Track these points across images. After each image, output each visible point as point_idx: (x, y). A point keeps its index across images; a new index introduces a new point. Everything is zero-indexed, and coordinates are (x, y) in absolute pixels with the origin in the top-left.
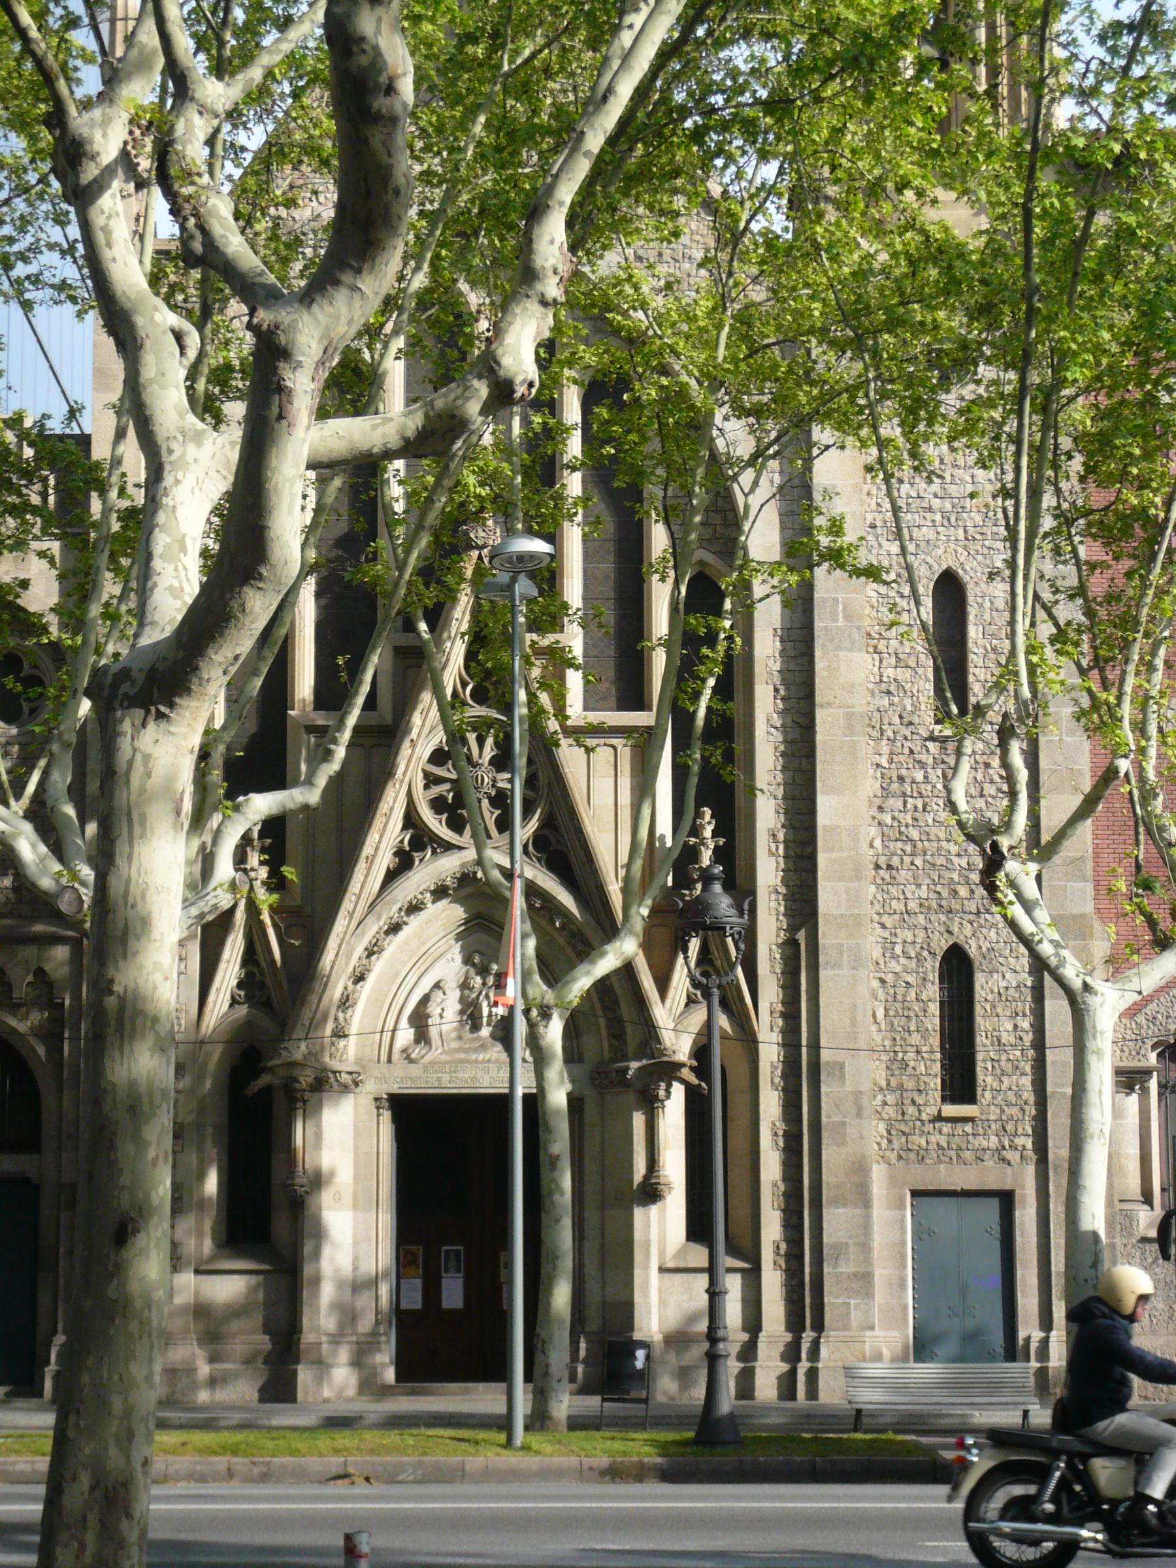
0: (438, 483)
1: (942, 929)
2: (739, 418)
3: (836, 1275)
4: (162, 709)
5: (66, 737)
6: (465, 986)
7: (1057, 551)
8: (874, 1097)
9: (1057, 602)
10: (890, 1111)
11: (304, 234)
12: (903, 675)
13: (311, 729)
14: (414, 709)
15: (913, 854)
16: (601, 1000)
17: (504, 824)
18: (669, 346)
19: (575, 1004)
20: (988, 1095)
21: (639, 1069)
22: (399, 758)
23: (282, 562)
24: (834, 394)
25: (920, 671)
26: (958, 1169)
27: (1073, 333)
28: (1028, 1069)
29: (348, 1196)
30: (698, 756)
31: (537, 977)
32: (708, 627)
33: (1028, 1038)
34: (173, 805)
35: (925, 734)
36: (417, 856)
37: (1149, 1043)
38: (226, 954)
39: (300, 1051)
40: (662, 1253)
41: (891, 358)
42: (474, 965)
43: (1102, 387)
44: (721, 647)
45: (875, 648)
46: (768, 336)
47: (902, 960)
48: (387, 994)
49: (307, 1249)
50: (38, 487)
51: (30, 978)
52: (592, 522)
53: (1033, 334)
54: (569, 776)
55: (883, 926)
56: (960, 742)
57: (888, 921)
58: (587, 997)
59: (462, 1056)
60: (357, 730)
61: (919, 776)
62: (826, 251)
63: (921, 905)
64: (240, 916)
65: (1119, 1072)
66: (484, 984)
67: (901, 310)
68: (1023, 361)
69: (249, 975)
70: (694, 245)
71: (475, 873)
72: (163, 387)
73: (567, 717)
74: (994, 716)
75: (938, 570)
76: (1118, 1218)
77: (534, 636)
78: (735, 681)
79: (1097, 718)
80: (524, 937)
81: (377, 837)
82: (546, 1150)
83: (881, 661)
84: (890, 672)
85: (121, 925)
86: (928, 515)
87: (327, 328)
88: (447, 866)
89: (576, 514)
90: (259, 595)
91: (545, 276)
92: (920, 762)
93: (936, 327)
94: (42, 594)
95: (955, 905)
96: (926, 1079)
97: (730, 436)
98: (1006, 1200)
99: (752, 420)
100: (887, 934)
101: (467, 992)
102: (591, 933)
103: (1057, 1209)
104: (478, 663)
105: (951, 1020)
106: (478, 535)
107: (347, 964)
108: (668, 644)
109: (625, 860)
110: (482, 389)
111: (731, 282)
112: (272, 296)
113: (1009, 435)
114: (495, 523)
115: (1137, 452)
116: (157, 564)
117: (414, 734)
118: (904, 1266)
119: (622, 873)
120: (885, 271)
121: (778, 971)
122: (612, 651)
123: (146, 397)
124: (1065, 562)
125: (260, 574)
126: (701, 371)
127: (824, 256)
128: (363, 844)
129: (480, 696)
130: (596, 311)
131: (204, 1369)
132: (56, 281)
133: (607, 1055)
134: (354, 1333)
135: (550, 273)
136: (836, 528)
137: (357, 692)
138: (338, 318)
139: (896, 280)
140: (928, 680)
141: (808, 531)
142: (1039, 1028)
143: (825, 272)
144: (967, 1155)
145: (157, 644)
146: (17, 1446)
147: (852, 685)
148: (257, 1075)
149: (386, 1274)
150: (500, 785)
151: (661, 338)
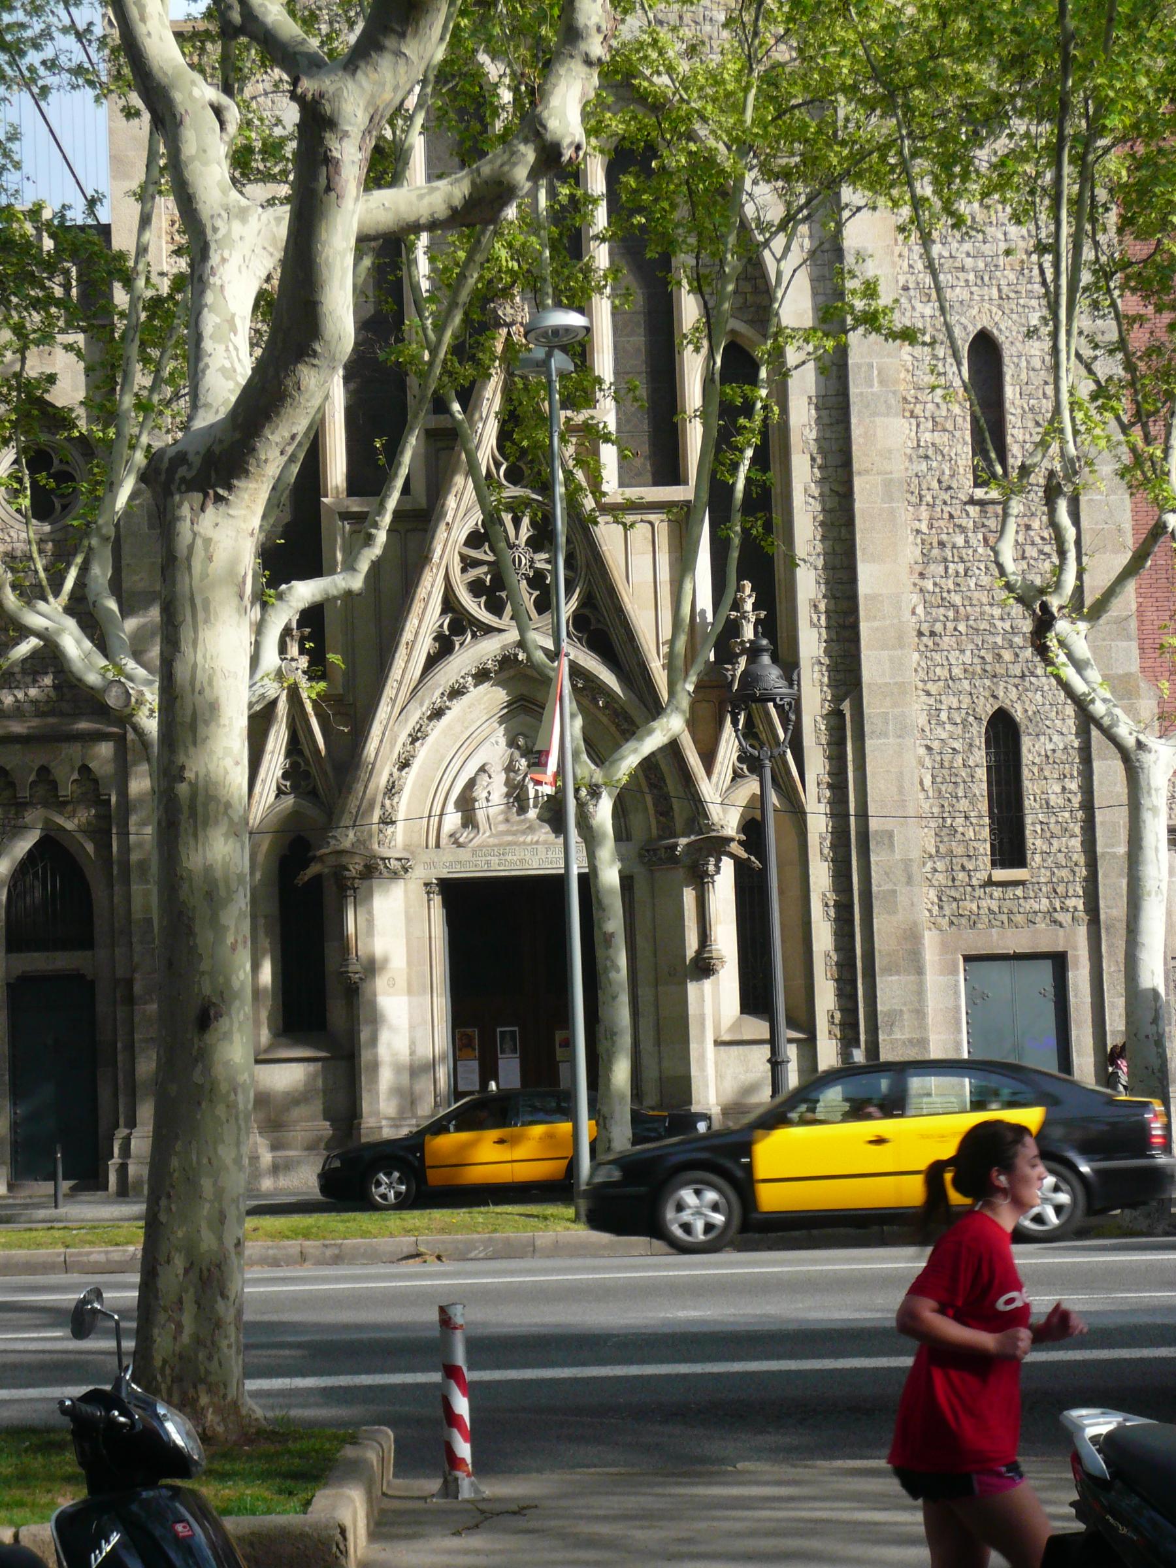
0: (470, 258)
1: (987, 694)
2: (768, 181)
3: (892, 1042)
4: (221, 491)
5: (104, 531)
6: (510, 768)
7: (1095, 305)
8: (924, 864)
9: (1096, 358)
10: (941, 878)
11: (320, 9)
12: (940, 438)
13: (345, 516)
14: (448, 492)
15: (955, 620)
16: (647, 777)
17: (544, 604)
18: (697, 111)
19: (624, 781)
20: (1038, 858)
21: (688, 845)
22: (435, 542)
24: (864, 155)
25: (958, 434)
26: (1009, 932)
28: (1077, 830)
29: (402, 983)
30: (738, 528)
31: (584, 757)
32: (745, 397)
33: (1077, 800)
34: (236, 589)
36: (457, 640)
38: (270, 746)
40: (717, 1027)
41: (923, 115)
42: (518, 747)
44: (758, 417)
45: (912, 412)
47: (948, 727)
49: (364, 1036)
50: (59, 279)
51: (75, 776)
53: (1070, 83)
54: (607, 554)
55: (928, 694)
57: (932, 688)
58: (633, 776)
59: (510, 838)
60: (397, 514)
61: (960, 540)
62: (856, 6)
63: (965, 671)
64: (282, 708)
67: (931, 64)
68: (1060, 113)
69: (294, 765)
71: (516, 655)
72: (206, 164)
74: (1038, 478)
75: (973, 331)
77: (569, 413)
78: (772, 452)
79: (1143, 474)
81: (416, 622)
82: (600, 928)
83: (918, 425)
84: (927, 437)
85: (189, 712)
87: (373, 96)
88: (488, 649)
89: (605, 286)
90: (313, 372)
91: (589, 35)
92: (960, 526)
93: (969, 79)
95: (1000, 670)
96: (975, 844)
97: (759, 201)
98: (1059, 961)
99: (780, 184)
100: (932, 701)
101: (512, 775)
102: (635, 712)
103: (1113, 969)
104: (513, 442)
105: (998, 784)
106: (506, 312)
107: (391, 751)
110: (529, 154)
111: (757, 42)
112: (314, 65)
113: (1043, 189)
114: (523, 299)
116: (208, 345)
117: (449, 518)
118: (959, 1031)
119: (665, 649)
120: (913, 25)
121: (824, 742)
123: (188, 175)
125: (315, 351)
126: (729, 134)
127: (853, 11)
128: (402, 630)
129: (514, 476)
130: (619, 77)
131: (267, 1158)
132: (73, 65)
133: (654, 832)
134: (414, 1116)
135: (593, 31)
136: (870, 290)
137: (396, 474)
138: (383, 84)
139: (925, 33)
141: (840, 294)
142: (1087, 790)
144: (1019, 918)
145: (212, 426)
146: (89, 1238)
147: (890, 451)
149: (444, 1058)
150: (538, 565)
151: (688, 103)
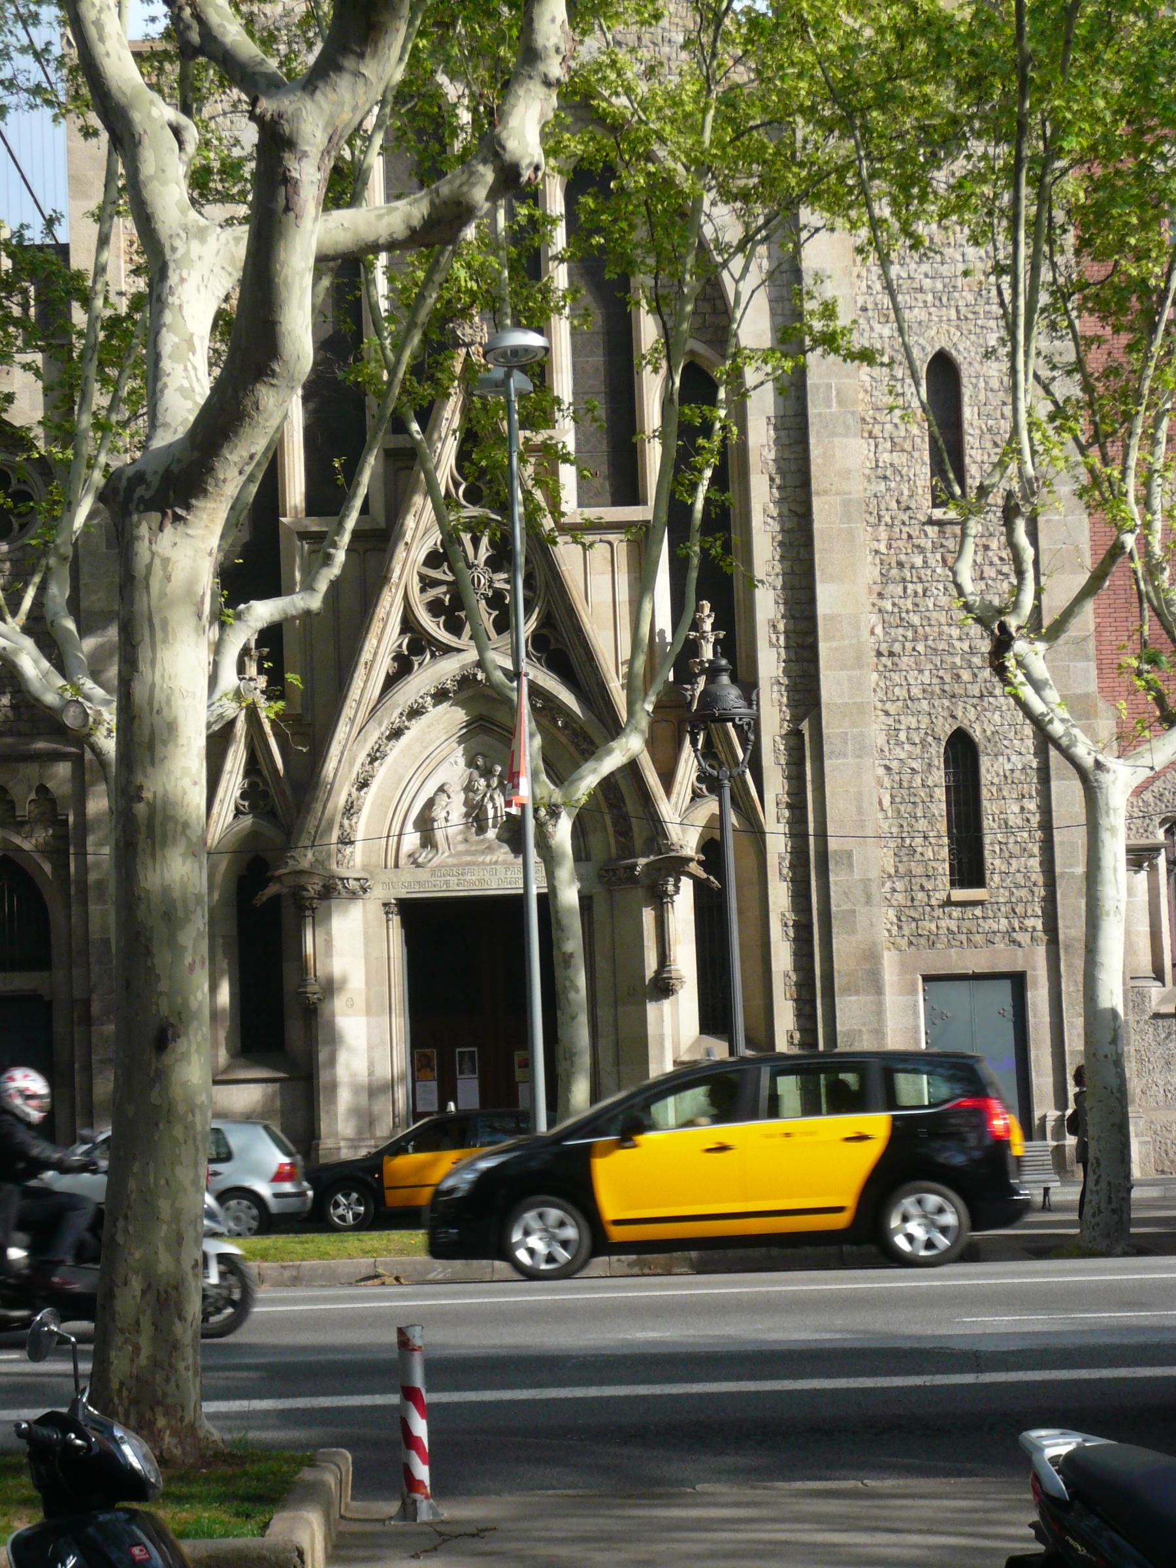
0: (429, 278)
1: (946, 714)
2: (727, 203)
4: (179, 511)
5: (62, 550)
6: (469, 788)
7: (1053, 326)
8: (883, 884)
9: (1054, 379)
10: (900, 898)
11: (278, 30)
12: (899, 459)
13: (304, 535)
14: (407, 511)
17: (503, 624)
18: (655, 132)
19: (583, 801)
20: (996, 878)
21: (647, 864)
22: (394, 562)
23: (295, 357)
24: (822, 176)
25: (916, 454)
26: (969, 952)
27: (1068, 102)
29: (360, 1003)
30: (697, 549)
31: (544, 777)
33: (1035, 820)
34: (194, 609)
35: (923, 519)
36: (416, 660)
37: (1157, 820)
38: (228, 766)
39: (307, 859)
40: (676, 1048)
41: (880, 137)
42: (477, 767)
43: (1096, 157)
44: (717, 438)
45: (870, 433)
46: (754, 118)
47: (907, 747)
48: (391, 800)
49: (322, 1056)
50: (17, 298)
51: (33, 796)
52: (580, 315)
53: (1027, 105)
54: (566, 574)
55: (887, 714)
56: (964, 525)
58: (592, 796)
59: (469, 858)
60: (356, 534)
61: (918, 561)
62: (814, 28)
63: (924, 691)
64: (241, 728)
65: (1130, 850)
66: (488, 786)
67: (889, 86)
68: (1018, 134)
70: (673, 28)
71: (475, 675)
73: (563, 514)
74: (996, 499)
75: (931, 352)
76: (1135, 997)
77: (528, 433)
78: (731, 472)
79: (1099, 494)
80: (532, 736)
81: (375, 642)
82: (559, 948)
83: (876, 446)
84: (885, 457)
85: (146, 732)
86: (919, 296)
87: (332, 117)
88: (447, 669)
89: (564, 307)
91: (548, 56)
92: (918, 547)
94: (28, 409)
95: (959, 690)
96: (934, 864)
97: (718, 222)
98: (1018, 981)
99: (738, 205)
100: (890, 721)
102: (594, 732)
103: (1071, 989)
104: (472, 462)
105: (957, 803)
106: (465, 332)
107: (350, 771)
108: (663, 435)
109: (628, 657)
111: (715, 63)
114: (482, 320)
115: (1134, 220)
116: (166, 364)
119: (624, 669)
120: (871, 46)
121: (783, 762)
122: (604, 446)
124: (1061, 338)
125: (273, 371)
126: (687, 155)
127: (811, 32)
128: (361, 650)
129: (473, 496)
130: (578, 98)
132: (31, 84)
133: (614, 851)
134: (373, 1137)
135: (552, 52)
136: (829, 311)
137: (354, 495)
139: (882, 55)
140: (924, 463)
141: (799, 315)
142: (1046, 810)
143: (813, 50)
144: (978, 938)
145: (170, 446)
147: (849, 472)
148: (265, 883)
149: (402, 1078)
150: (497, 585)
151: (646, 124)
